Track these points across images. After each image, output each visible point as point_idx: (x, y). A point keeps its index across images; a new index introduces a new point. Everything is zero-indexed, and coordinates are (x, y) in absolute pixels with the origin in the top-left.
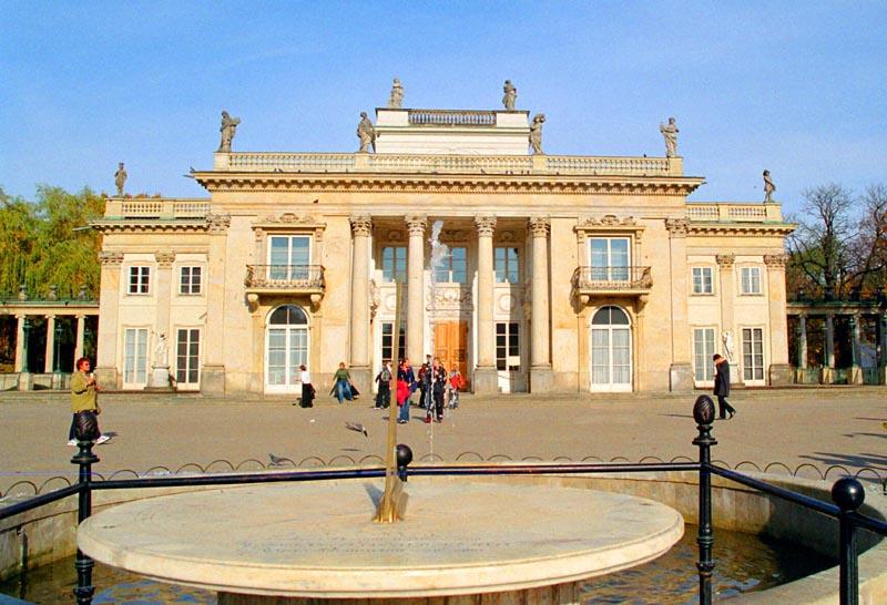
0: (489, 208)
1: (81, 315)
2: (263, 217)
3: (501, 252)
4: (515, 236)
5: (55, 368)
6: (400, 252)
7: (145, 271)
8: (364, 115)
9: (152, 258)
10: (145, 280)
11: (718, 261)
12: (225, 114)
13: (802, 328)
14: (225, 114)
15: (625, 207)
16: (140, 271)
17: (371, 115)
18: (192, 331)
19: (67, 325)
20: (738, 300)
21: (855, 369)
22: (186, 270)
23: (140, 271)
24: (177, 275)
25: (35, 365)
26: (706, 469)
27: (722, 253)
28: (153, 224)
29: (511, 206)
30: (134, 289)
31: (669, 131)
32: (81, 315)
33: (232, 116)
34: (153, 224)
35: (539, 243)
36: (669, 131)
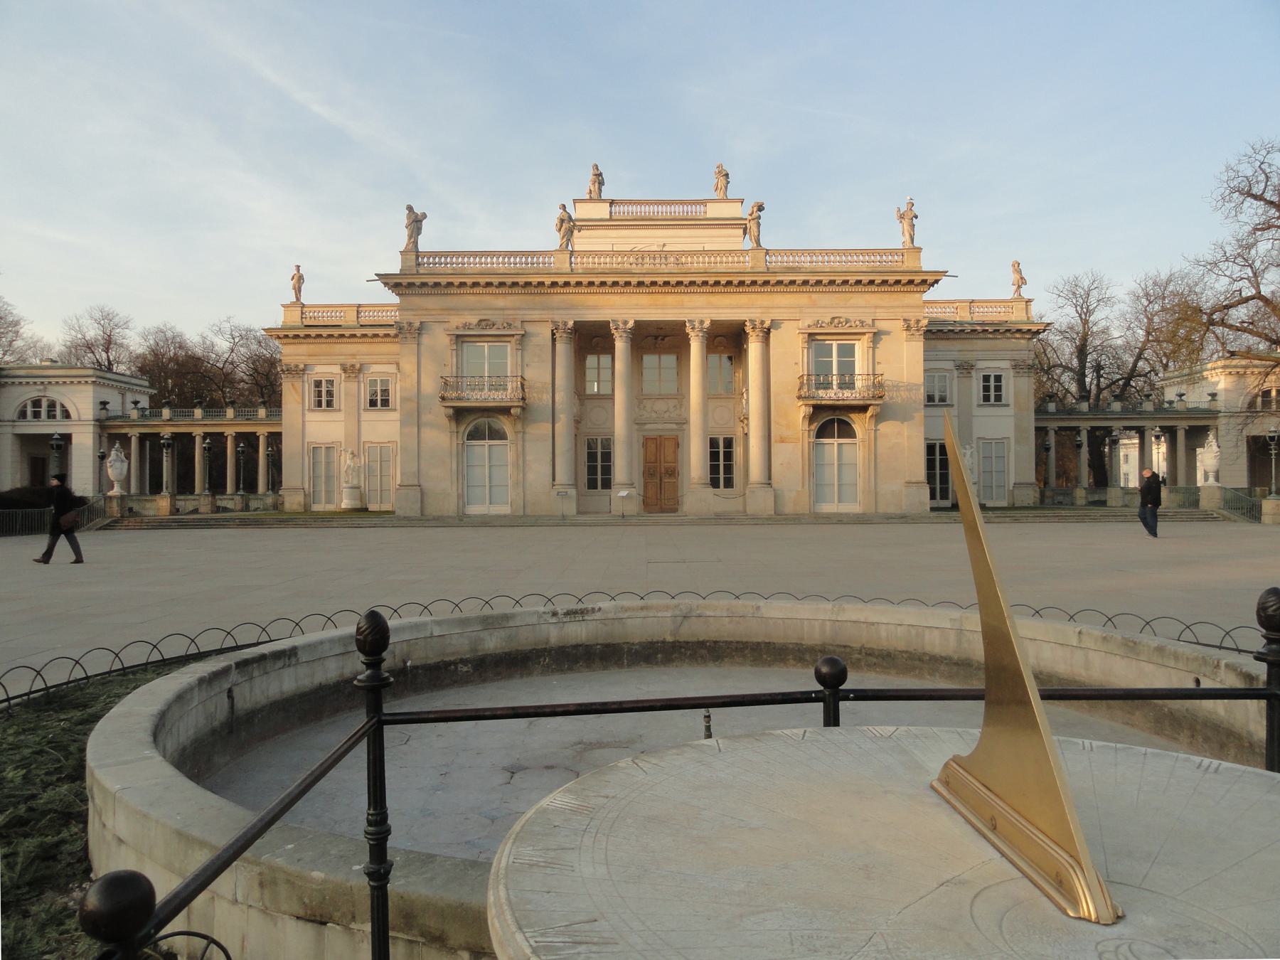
0: (699, 311)
1: (262, 431)
2: (809, 322)
3: (714, 358)
4: (729, 341)
5: (237, 488)
6: (605, 359)
7: (998, 378)
8: (564, 207)
9: (1006, 364)
10: (998, 388)
11: (345, 370)
12: (410, 208)
13: (1052, 440)
14: (410, 208)
15: (857, 307)
16: (992, 379)
17: (570, 209)
18: (725, 439)
19: (249, 440)
20: (977, 412)
21: (1134, 483)
22: (318, 384)
23: (992, 379)
24: (976, 386)
25: (216, 485)
26: (77, 662)
27: (350, 361)
28: (336, 332)
29: (728, 308)
30: (986, 398)
31: (909, 217)
32: (262, 431)
33: (418, 211)
34: (336, 332)
35: (754, 348)
36: (909, 217)
